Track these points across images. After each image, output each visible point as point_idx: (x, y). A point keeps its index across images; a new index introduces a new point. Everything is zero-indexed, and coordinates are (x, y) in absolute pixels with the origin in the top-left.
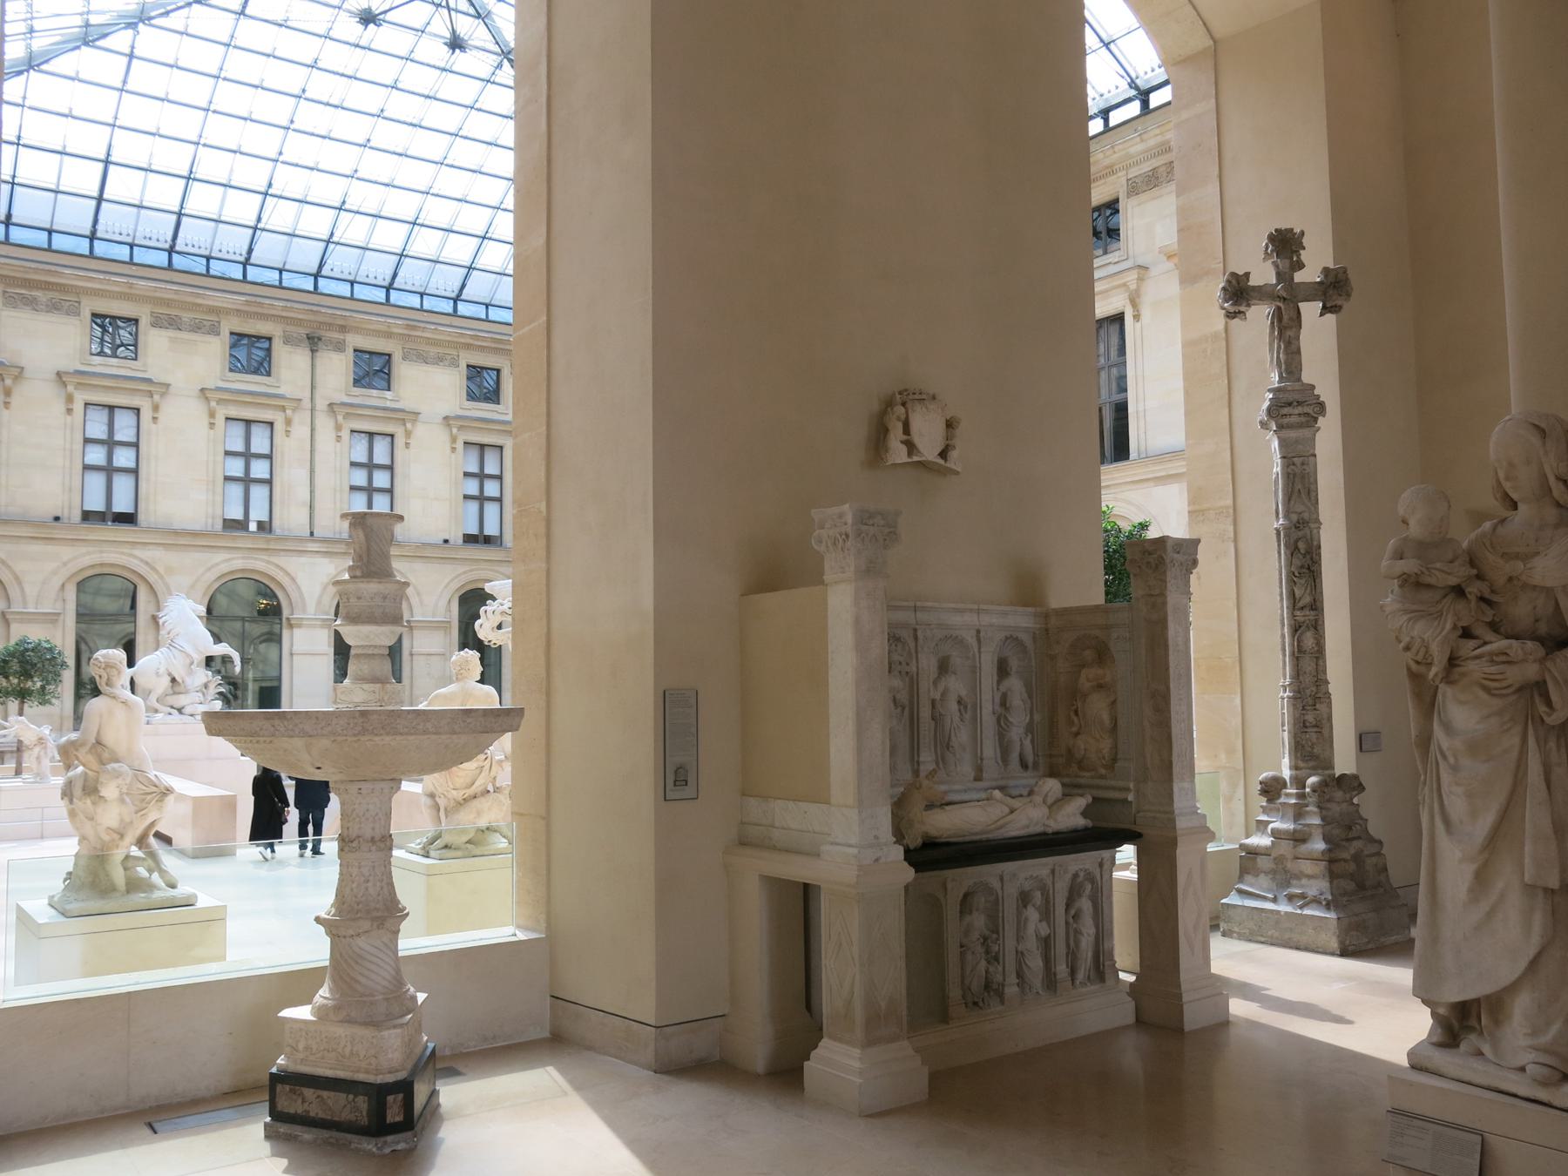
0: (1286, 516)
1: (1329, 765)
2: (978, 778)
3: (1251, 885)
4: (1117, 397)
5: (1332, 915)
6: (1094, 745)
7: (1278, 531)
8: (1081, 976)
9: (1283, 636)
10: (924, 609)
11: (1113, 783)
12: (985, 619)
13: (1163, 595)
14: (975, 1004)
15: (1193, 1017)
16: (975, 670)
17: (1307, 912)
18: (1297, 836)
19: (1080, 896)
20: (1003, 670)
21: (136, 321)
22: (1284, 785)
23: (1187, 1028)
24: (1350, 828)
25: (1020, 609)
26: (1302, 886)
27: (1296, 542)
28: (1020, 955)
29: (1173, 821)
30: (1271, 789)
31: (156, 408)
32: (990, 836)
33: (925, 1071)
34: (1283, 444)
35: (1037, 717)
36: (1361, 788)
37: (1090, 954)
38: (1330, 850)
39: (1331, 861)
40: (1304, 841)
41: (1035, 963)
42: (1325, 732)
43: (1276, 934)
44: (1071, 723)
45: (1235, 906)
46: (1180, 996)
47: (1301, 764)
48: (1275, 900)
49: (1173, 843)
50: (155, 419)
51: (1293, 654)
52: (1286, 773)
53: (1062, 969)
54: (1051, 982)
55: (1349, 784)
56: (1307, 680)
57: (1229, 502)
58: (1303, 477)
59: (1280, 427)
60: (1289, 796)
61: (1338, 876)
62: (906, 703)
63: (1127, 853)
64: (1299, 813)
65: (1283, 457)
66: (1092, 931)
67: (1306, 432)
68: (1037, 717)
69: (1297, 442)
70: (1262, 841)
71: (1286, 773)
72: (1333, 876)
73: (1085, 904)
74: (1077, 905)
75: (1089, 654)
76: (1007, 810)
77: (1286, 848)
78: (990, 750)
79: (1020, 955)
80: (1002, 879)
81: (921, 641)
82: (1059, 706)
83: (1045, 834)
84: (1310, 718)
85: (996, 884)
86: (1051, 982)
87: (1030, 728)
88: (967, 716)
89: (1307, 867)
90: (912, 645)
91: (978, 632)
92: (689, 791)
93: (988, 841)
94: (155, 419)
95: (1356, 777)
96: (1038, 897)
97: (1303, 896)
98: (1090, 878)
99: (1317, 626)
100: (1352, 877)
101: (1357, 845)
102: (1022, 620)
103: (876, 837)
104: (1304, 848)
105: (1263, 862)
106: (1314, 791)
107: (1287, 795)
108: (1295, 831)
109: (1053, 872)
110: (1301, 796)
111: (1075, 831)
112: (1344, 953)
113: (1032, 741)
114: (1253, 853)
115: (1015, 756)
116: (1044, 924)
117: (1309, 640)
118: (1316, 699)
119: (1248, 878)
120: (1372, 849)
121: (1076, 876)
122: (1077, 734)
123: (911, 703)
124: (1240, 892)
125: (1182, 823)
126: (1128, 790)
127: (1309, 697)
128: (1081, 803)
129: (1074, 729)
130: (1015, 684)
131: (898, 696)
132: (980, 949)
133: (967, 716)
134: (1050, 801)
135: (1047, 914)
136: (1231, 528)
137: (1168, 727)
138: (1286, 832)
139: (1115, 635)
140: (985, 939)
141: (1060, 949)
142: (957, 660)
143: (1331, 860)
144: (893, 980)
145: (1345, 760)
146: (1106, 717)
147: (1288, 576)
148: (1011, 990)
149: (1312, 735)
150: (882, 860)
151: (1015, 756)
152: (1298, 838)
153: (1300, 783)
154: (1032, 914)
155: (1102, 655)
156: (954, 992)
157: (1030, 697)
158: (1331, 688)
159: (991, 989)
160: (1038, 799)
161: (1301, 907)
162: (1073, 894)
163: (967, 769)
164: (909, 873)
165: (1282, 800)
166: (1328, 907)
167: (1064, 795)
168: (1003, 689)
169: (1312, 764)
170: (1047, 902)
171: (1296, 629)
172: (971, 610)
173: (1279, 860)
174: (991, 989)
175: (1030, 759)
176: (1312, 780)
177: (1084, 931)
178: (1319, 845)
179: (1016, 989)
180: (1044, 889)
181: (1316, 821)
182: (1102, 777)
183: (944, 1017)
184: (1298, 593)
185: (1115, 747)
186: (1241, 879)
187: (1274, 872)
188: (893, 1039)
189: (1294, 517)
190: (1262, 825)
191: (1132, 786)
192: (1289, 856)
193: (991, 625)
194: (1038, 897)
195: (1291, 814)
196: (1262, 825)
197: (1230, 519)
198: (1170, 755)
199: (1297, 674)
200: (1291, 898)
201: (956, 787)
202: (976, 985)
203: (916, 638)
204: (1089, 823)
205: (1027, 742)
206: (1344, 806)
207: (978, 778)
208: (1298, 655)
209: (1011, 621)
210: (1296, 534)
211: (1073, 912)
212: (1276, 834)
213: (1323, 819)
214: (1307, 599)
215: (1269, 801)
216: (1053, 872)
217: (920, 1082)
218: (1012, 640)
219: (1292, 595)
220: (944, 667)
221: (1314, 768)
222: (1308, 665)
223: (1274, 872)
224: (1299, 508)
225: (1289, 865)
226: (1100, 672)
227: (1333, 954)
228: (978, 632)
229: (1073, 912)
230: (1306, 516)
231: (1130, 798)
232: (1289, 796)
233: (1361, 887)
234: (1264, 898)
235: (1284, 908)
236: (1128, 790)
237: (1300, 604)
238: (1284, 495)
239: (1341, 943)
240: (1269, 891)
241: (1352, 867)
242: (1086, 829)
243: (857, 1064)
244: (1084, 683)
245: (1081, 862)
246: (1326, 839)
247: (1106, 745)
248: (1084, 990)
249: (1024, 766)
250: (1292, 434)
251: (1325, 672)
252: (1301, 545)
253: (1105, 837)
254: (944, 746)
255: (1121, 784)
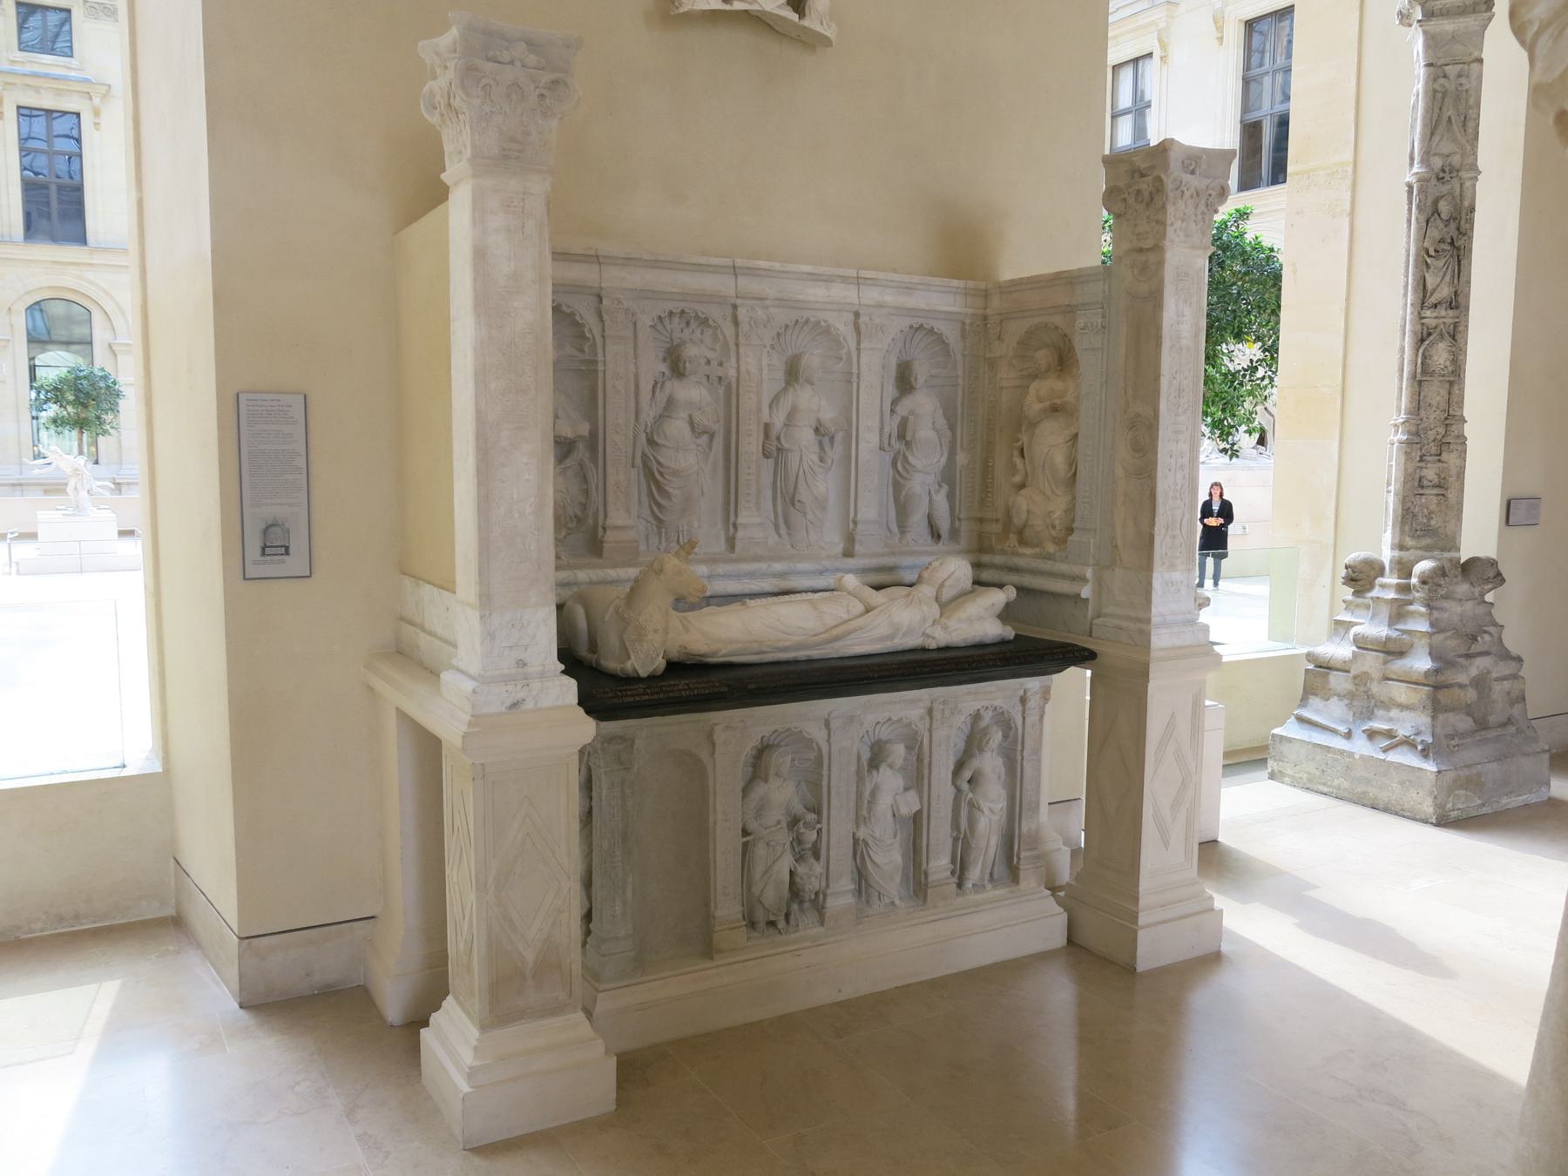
0: (1425, 160)
1: (1452, 544)
2: (848, 554)
3: (1317, 711)
4: (1279, 108)
5: (1430, 767)
6: (1040, 505)
7: (1410, 187)
8: (974, 874)
9: (1402, 350)
10: (752, 272)
11: (1063, 568)
12: (871, 295)
13: (1158, 248)
14: (772, 924)
15: (1155, 947)
16: (850, 379)
17: (1393, 757)
18: (1391, 647)
19: (981, 750)
20: (905, 382)
21: (69, 11)
22: (1381, 572)
23: (1142, 965)
24: (1474, 639)
25: (937, 281)
26: (1391, 720)
27: (1436, 202)
28: (859, 849)
29: (1146, 635)
30: (1360, 578)
31: (97, 113)
32: (815, 653)
33: (612, 1063)
34: (1432, 42)
35: (962, 459)
36: (1499, 579)
37: (994, 841)
38: (1437, 671)
39: (1436, 688)
40: (1401, 654)
41: (888, 858)
42: (1451, 495)
43: (1346, 784)
44: (1012, 469)
45: (1290, 740)
46: (1134, 917)
47: (1409, 542)
48: (1348, 735)
49: (1143, 674)
50: (96, 124)
51: (1414, 376)
52: (1386, 555)
53: (939, 864)
54: (918, 885)
55: (1482, 572)
56: (1432, 416)
57: (1348, 156)
58: (1458, 98)
59: (1429, 15)
60: (1386, 588)
61: (1447, 709)
62: (719, 428)
63: (1076, 682)
64: (1398, 613)
65: (1429, 65)
66: (1000, 805)
67: (1470, 22)
68: (962, 459)
69: (1454, 38)
70: (1341, 650)
71: (1386, 555)
72: (1436, 708)
73: (990, 763)
74: (975, 763)
75: (1043, 357)
76: (861, 608)
77: (1371, 663)
78: (872, 507)
79: (859, 849)
80: (827, 724)
81: (744, 327)
82: (992, 442)
83: (924, 650)
84: (1430, 473)
85: (817, 733)
86: (918, 885)
87: (948, 477)
88: (835, 453)
89: (1401, 692)
90: (728, 329)
91: (857, 315)
92: (295, 562)
93: (810, 661)
94: (96, 124)
95: (1492, 563)
96: (898, 752)
97: (1389, 734)
98: (1006, 724)
99: (1455, 335)
100: (1468, 710)
101: (1481, 663)
102: (943, 301)
103: (522, 664)
104: (1399, 665)
105: (1337, 681)
106: (1424, 583)
107: (1383, 586)
108: (1388, 639)
109: (930, 712)
110: (1405, 589)
111: (981, 646)
112: (1443, 822)
113: (951, 497)
114: (1324, 667)
115: (918, 519)
116: (912, 794)
117: (1441, 355)
118: (1442, 445)
119: (1315, 701)
120: (1505, 668)
121: (977, 717)
122: (1022, 486)
123: (728, 431)
124: (1301, 719)
125: (1160, 640)
126: (1084, 580)
127: (1433, 439)
128: (998, 598)
129: (1018, 479)
130: (924, 405)
131: (697, 417)
132: (784, 837)
133: (835, 453)
134: (947, 594)
135: (918, 777)
136: (1348, 196)
137: (1152, 477)
138: (1376, 641)
139: (1080, 322)
140: (794, 822)
141: (940, 834)
142: (813, 359)
143: (1437, 686)
144: (549, 905)
145: (1479, 534)
146: (1059, 459)
147: (1417, 255)
148: (841, 898)
149: (1430, 499)
150: (529, 705)
151: (918, 519)
152: (1392, 650)
153: (1404, 569)
154: (890, 781)
155: (1064, 360)
156: (727, 909)
157: (952, 428)
158: (1468, 430)
159: (800, 899)
160: (926, 591)
161: (1385, 750)
162: (973, 743)
163: (833, 539)
164: (586, 728)
165: (1375, 593)
166: (1425, 753)
167: (977, 582)
168: (902, 410)
169: (1427, 541)
170: (920, 759)
171: (1423, 338)
172: (845, 279)
173: (1361, 679)
174: (800, 899)
175: (944, 525)
176: (1424, 566)
177: (984, 805)
178: (1421, 663)
179: (849, 900)
180: (913, 743)
181: (1422, 626)
182: (1049, 557)
183: (708, 950)
184: (1431, 281)
185: (1071, 510)
186: (1304, 702)
187: (1351, 696)
188: (556, 1010)
189: (1437, 163)
190: (1340, 627)
191: (1089, 574)
192: (1376, 675)
193: (880, 306)
194: (898, 752)
195: (1385, 613)
196: (1340, 627)
197: (1349, 182)
198: (1153, 524)
199: (1418, 405)
200: (1372, 735)
201: (801, 566)
202: (772, 893)
203: (736, 323)
204: (1009, 633)
205: (941, 499)
206: (1469, 605)
207: (848, 554)
208: (1422, 377)
209: (918, 301)
210: (1436, 189)
211: (967, 774)
212: (1362, 643)
213: (1432, 625)
214: (1445, 292)
215: (1357, 593)
216: (930, 712)
217: (598, 1087)
218: (921, 330)
219: (1422, 285)
220: (793, 373)
221: (1428, 548)
222: (1435, 393)
223: (1351, 696)
224: (1446, 147)
225: (1375, 688)
226: (1058, 385)
227: (1425, 821)
228: (857, 315)
229: (967, 774)
230: (1456, 160)
231: (1086, 592)
232: (1386, 588)
233: (1482, 725)
234: (1334, 731)
235: (1361, 747)
236: (1084, 580)
237: (1433, 300)
238: (1424, 125)
239: (1439, 806)
240: (1343, 721)
241: (1471, 695)
242: (1003, 642)
243: (468, 1058)
244: (1033, 406)
245: (995, 694)
246: (1434, 654)
247: (1058, 507)
248: (979, 897)
249: (936, 535)
250: (1447, 26)
251: (1461, 404)
252: (1444, 207)
253: (1028, 654)
254: (788, 500)
255: (1076, 569)
